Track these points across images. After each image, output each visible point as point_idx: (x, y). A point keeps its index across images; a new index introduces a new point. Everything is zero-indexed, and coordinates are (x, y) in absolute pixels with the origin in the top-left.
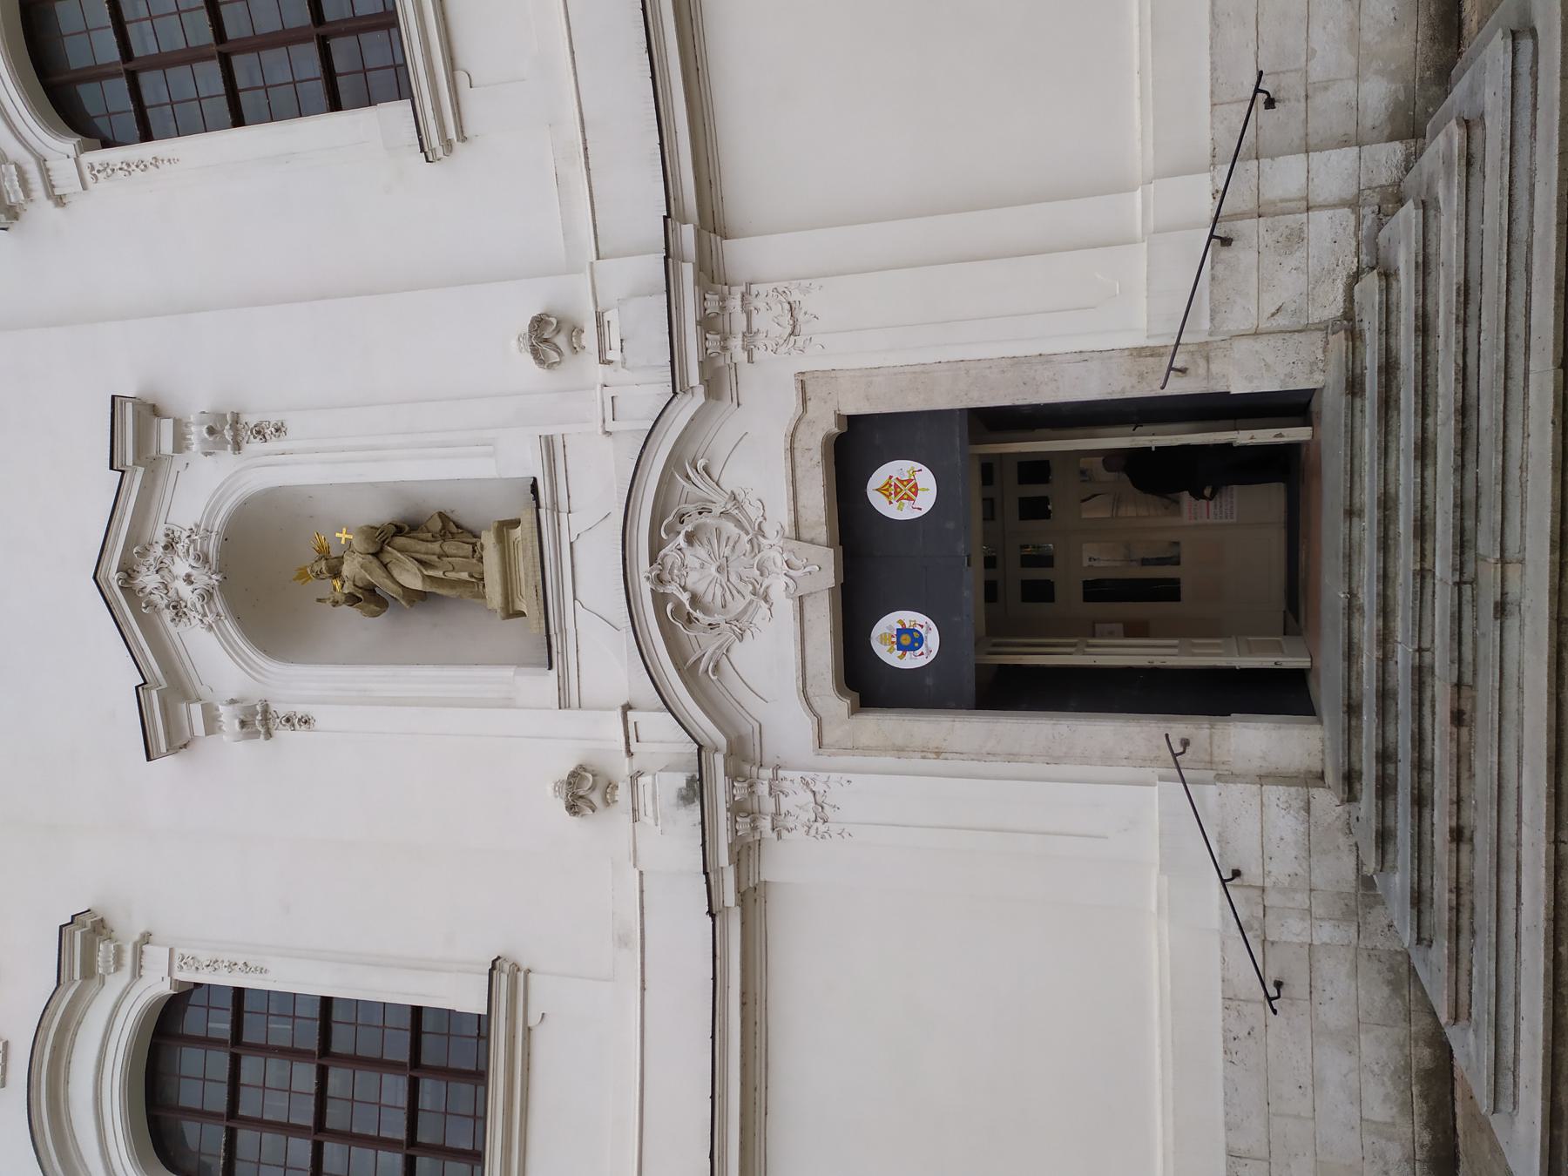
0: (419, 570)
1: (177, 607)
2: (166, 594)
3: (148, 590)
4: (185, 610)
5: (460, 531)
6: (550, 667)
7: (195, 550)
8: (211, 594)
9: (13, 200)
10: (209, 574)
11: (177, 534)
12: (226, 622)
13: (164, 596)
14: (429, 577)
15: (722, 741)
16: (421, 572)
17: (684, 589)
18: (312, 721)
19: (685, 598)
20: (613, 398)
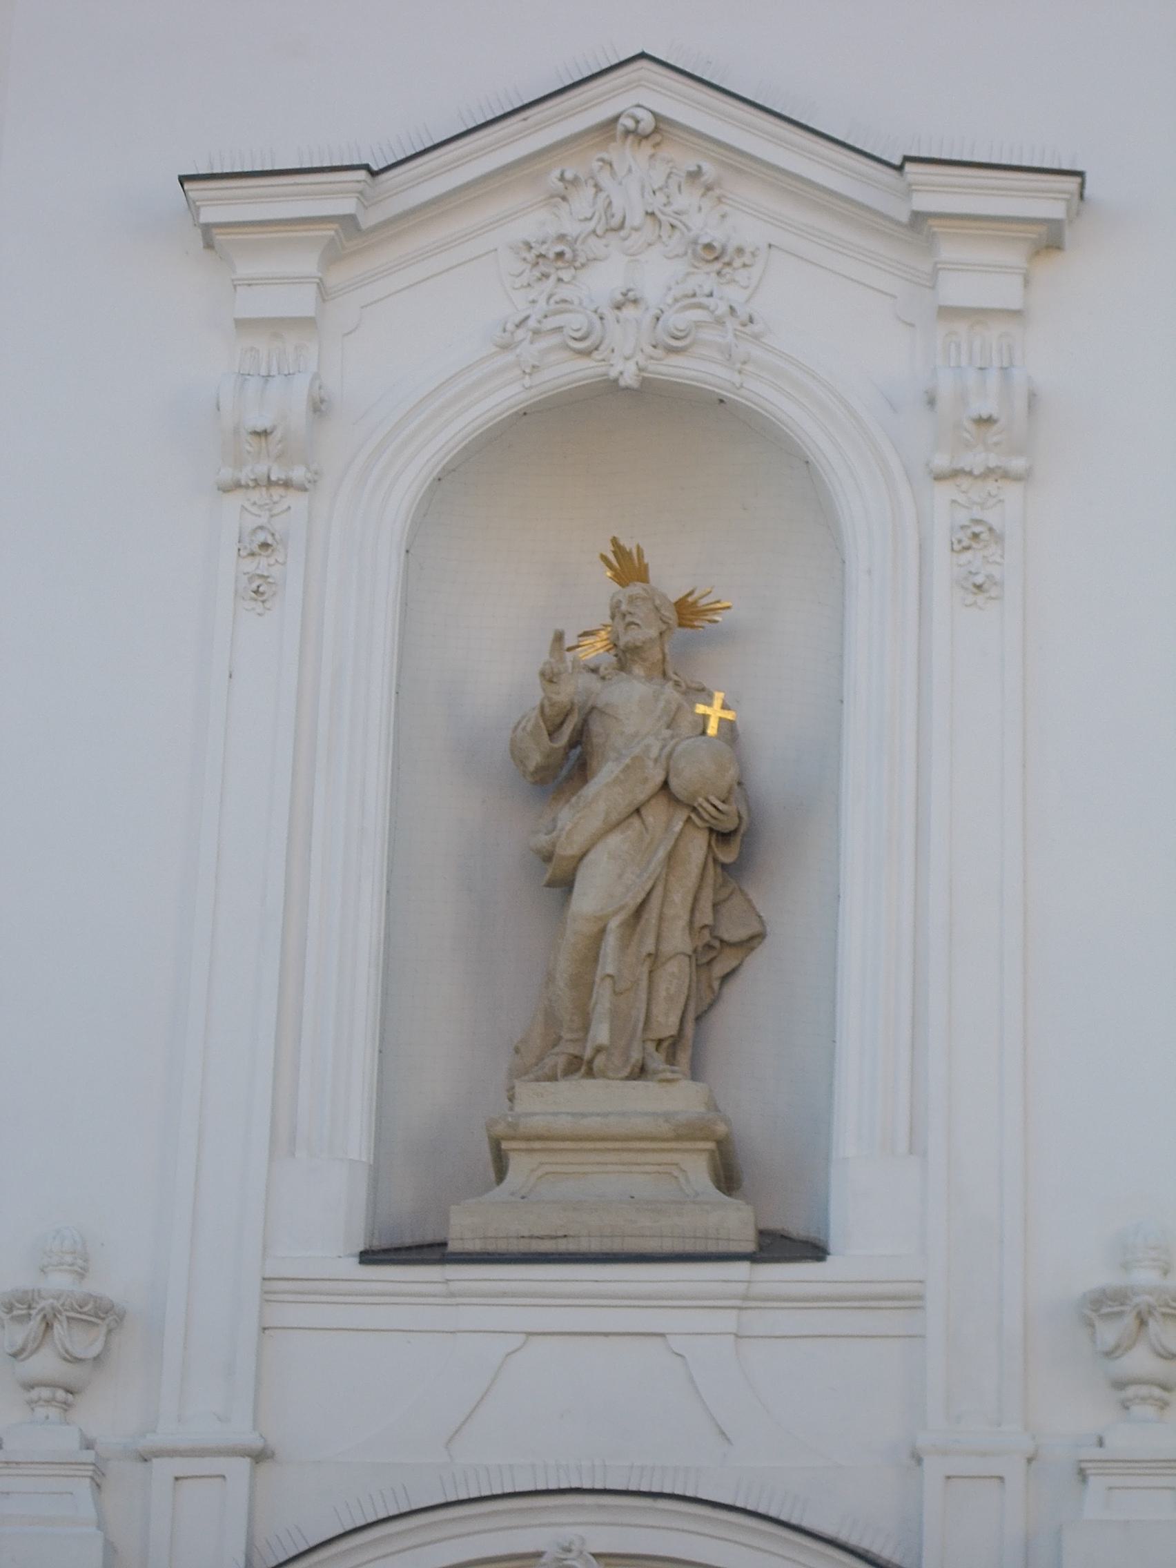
0: (622, 908)
2: (594, 232)
3: (605, 179)
4: (553, 279)
5: (716, 984)
6: (368, 1257)
7: (698, 325)
8: (587, 353)
10: (640, 358)
11: (741, 276)
12: (516, 388)
13: (592, 225)
14: (603, 931)
16: (615, 913)
18: (259, 607)
20: (1001, 1478)
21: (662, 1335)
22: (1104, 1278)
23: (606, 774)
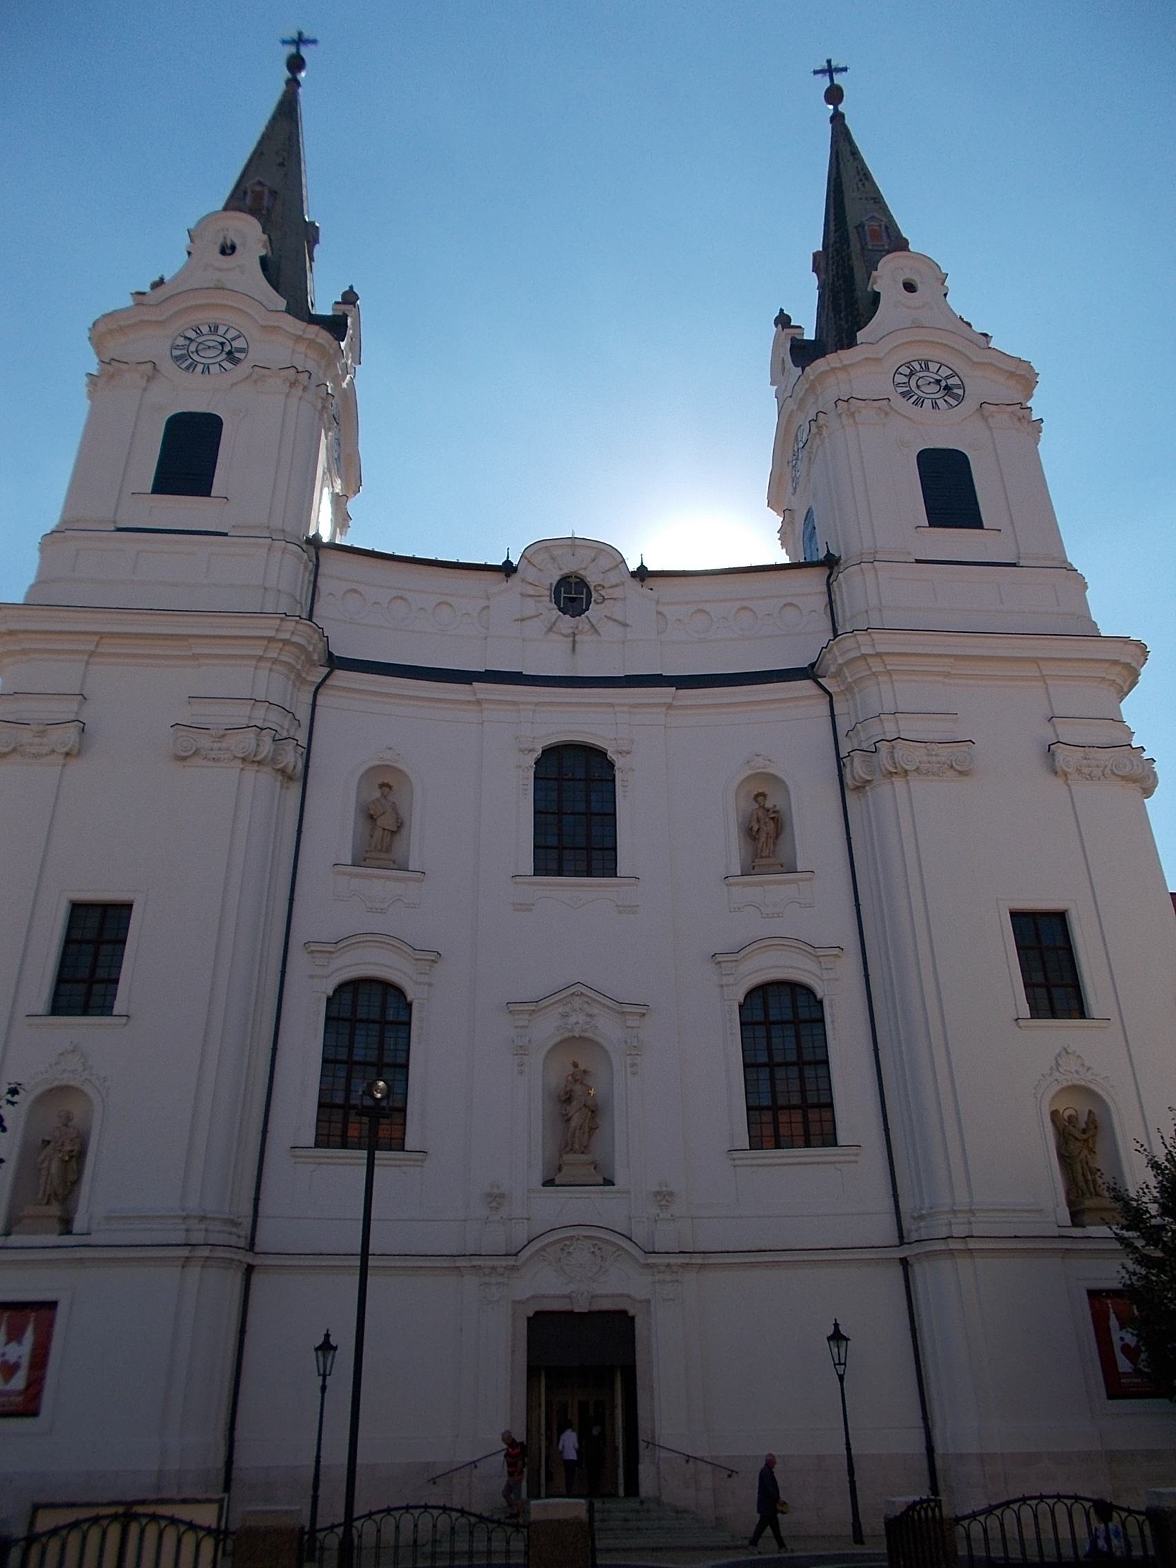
1: (565, 1016)
9: (383, 1126)
15: (519, 1263)
17: (574, 1249)
19: (571, 1249)
21: (119, 530)
22: (657, 1189)
23: (574, 1103)
